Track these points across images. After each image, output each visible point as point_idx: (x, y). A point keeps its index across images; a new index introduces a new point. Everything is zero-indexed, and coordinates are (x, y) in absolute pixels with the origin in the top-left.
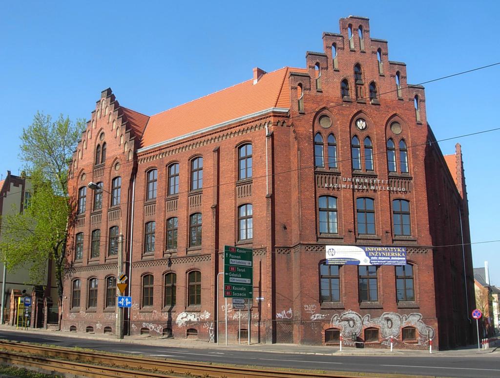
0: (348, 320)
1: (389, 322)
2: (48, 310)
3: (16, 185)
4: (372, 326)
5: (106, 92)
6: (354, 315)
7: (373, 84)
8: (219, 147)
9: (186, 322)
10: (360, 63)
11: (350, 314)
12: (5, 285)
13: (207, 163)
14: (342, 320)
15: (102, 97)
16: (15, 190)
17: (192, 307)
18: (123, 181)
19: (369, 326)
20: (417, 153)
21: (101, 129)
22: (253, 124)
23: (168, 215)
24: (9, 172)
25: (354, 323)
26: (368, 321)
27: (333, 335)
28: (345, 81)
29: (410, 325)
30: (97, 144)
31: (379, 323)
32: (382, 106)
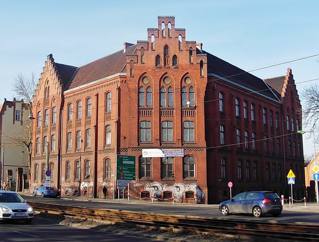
0: (154, 187)
1: (178, 188)
2: (24, 181)
3: (10, 107)
4: (168, 190)
5: (49, 56)
6: (158, 184)
7: (175, 57)
8: (98, 94)
9: (84, 187)
10: (168, 44)
11: (157, 184)
12: (3, 167)
13: (93, 101)
14: (151, 187)
15: (47, 59)
16: (9, 111)
17: (86, 180)
18: (57, 110)
19: (166, 191)
20: (200, 94)
21: (47, 79)
22: (112, 81)
23: (107, 123)
24: (5, 99)
25: (158, 188)
26: (166, 187)
27: (146, 195)
28: (158, 57)
29: (190, 190)
30: (46, 87)
31: (172, 189)
32: (180, 69)
